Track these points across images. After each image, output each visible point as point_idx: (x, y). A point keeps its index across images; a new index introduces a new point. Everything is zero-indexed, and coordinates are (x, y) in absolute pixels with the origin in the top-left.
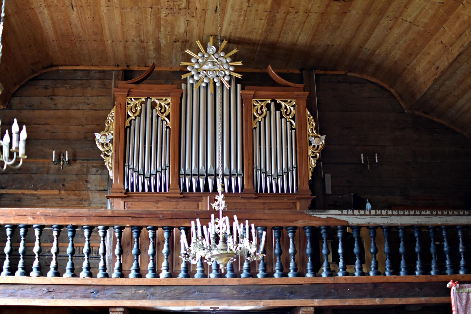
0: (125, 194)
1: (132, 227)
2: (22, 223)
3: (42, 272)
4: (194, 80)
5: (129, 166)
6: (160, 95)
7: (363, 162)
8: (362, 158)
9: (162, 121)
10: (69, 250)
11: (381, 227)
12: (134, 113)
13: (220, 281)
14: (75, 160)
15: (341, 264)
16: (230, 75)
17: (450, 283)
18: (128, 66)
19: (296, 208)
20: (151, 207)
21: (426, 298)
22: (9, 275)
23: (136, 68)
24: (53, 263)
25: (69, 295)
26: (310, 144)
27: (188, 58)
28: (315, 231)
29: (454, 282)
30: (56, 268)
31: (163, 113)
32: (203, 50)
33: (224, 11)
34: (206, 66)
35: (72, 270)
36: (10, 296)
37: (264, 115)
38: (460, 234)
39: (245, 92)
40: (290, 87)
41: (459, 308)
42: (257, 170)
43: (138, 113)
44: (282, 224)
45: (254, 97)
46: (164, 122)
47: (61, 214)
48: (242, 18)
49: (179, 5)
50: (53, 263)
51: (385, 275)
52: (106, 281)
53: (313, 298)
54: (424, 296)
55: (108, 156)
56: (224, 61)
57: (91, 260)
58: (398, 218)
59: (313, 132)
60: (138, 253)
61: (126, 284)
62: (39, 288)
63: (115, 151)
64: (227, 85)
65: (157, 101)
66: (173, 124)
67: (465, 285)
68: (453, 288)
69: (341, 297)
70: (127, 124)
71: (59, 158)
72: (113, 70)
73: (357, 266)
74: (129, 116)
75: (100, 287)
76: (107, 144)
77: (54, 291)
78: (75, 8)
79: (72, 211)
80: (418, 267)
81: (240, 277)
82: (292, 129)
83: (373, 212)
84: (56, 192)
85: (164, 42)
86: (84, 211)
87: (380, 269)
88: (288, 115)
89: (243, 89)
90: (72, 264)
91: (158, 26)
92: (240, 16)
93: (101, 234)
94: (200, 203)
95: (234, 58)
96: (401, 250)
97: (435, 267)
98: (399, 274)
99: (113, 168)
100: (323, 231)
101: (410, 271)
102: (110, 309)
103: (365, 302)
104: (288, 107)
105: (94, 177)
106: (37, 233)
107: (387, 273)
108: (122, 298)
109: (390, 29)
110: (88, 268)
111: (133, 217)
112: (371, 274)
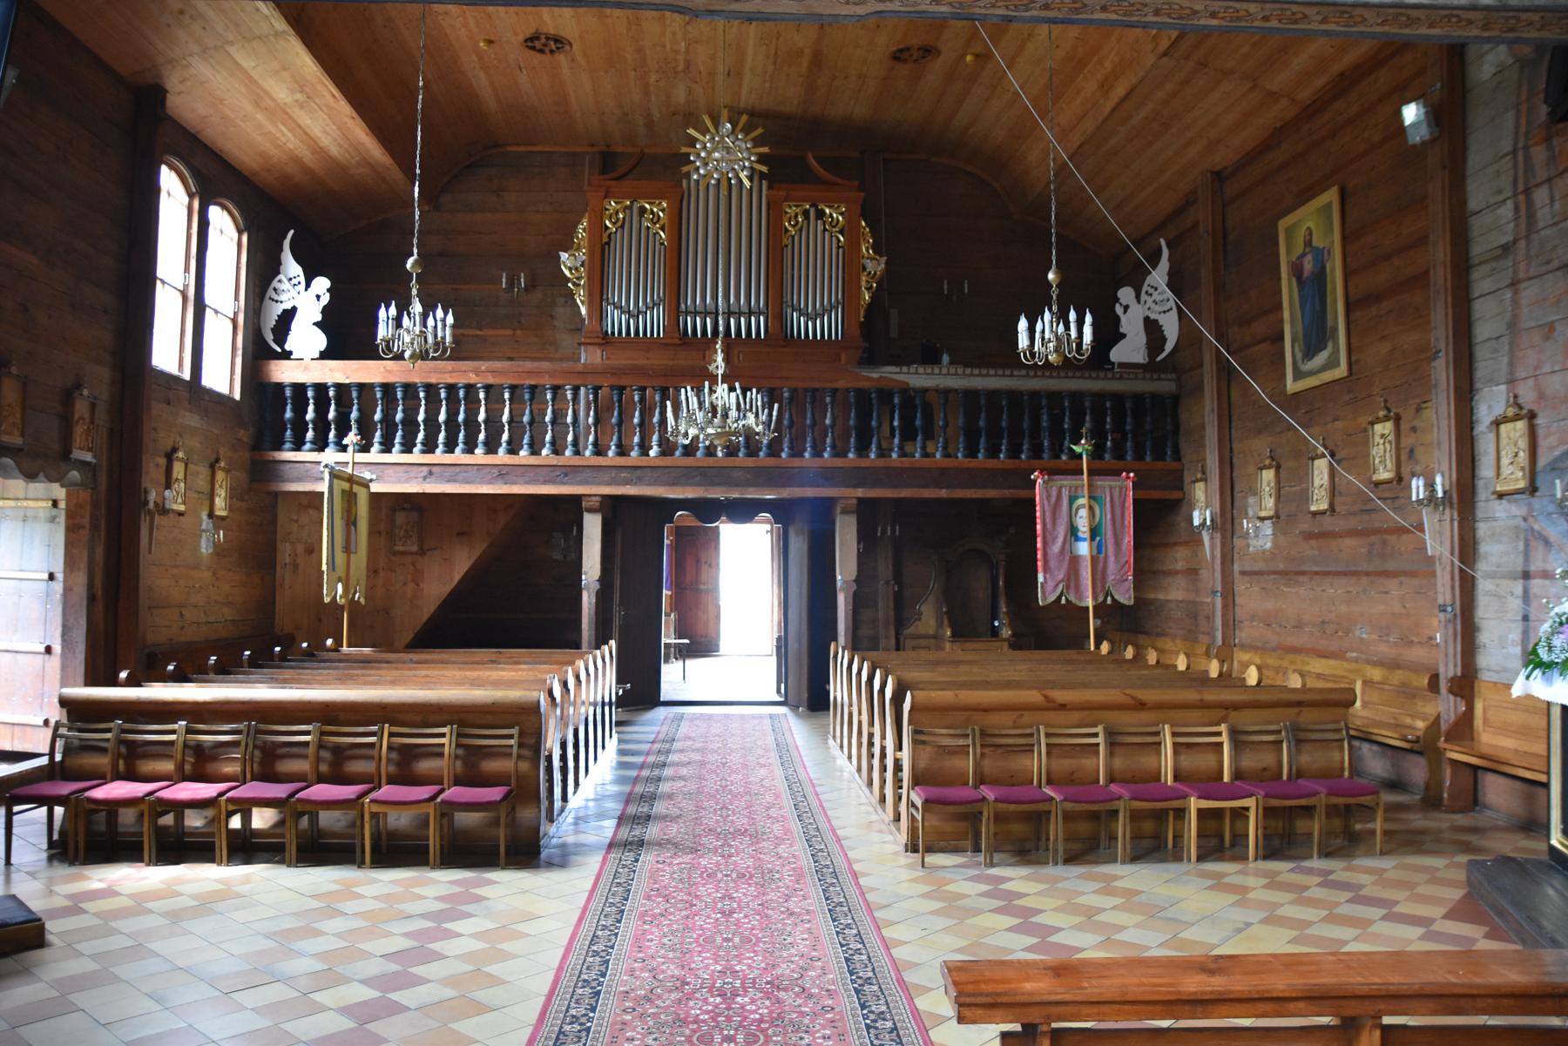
0: (603, 339)
1: (612, 387)
2: (461, 380)
3: (491, 447)
4: (699, 174)
5: (608, 299)
6: (651, 197)
7: (946, 292)
8: (946, 287)
9: (655, 234)
10: (526, 419)
11: (956, 391)
12: (614, 224)
13: (731, 461)
14: (534, 287)
15: (896, 441)
16: (752, 168)
17: (1036, 474)
18: (608, 146)
19: (840, 360)
20: (639, 359)
21: (1011, 491)
22: (446, 452)
23: (620, 149)
24: (505, 437)
25: (527, 479)
26: (864, 269)
27: (692, 142)
28: (862, 394)
29: (1041, 473)
30: (509, 443)
31: (655, 224)
32: (712, 129)
33: (740, 75)
34: (716, 154)
35: (531, 445)
36: (449, 481)
37: (799, 226)
38: (1066, 404)
39: (774, 192)
40: (837, 184)
41: (1046, 507)
42: (787, 306)
43: (619, 224)
44: (817, 385)
45: (786, 200)
46: (657, 236)
47: (515, 370)
48: (767, 85)
49: (674, 68)
50: (505, 437)
51: (957, 457)
52: (577, 461)
53: (856, 486)
54: (1009, 488)
55: (579, 285)
56: (743, 146)
57: (557, 428)
58: (980, 379)
59: (868, 251)
60: (620, 424)
61: (604, 464)
62: (487, 470)
63: (589, 279)
64: (747, 183)
65: (647, 206)
66: (669, 237)
67: (1056, 477)
68: (1039, 481)
69: (895, 486)
70: (605, 239)
71: (511, 284)
72: (587, 153)
73: (919, 445)
74: (607, 228)
75: (569, 469)
76: (576, 269)
77: (507, 474)
78: (525, 72)
79: (529, 365)
80: (1003, 447)
81: (758, 456)
82: (839, 247)
83: (952, 371)
84: (509, 332)
85: (658, 116)
86: (545, 365)
87: (950, 450)
88: (834, 227)
89: (770, 187)
90: (531, 437)
91: (647, 93)
92: (764, 81)
93: (569, 395)
94: (707, 353)
95: (757, 142)
96: (982, 424)
97: (1028, 449)
98: (977, 457)
99: (586, 303)
100: (873, 395)
101: (993, 452)
102: (583, 498)
103: (928, 493)
104: (835, 215)
105: (560, 311)
106: (482, 395)
107: (960, 455)
108: (599, 484)
109: (987, 100)
110: (553, 443)
111: (613, 374)
112: (938, 455)
